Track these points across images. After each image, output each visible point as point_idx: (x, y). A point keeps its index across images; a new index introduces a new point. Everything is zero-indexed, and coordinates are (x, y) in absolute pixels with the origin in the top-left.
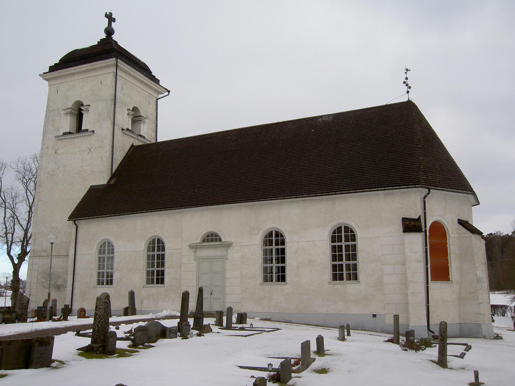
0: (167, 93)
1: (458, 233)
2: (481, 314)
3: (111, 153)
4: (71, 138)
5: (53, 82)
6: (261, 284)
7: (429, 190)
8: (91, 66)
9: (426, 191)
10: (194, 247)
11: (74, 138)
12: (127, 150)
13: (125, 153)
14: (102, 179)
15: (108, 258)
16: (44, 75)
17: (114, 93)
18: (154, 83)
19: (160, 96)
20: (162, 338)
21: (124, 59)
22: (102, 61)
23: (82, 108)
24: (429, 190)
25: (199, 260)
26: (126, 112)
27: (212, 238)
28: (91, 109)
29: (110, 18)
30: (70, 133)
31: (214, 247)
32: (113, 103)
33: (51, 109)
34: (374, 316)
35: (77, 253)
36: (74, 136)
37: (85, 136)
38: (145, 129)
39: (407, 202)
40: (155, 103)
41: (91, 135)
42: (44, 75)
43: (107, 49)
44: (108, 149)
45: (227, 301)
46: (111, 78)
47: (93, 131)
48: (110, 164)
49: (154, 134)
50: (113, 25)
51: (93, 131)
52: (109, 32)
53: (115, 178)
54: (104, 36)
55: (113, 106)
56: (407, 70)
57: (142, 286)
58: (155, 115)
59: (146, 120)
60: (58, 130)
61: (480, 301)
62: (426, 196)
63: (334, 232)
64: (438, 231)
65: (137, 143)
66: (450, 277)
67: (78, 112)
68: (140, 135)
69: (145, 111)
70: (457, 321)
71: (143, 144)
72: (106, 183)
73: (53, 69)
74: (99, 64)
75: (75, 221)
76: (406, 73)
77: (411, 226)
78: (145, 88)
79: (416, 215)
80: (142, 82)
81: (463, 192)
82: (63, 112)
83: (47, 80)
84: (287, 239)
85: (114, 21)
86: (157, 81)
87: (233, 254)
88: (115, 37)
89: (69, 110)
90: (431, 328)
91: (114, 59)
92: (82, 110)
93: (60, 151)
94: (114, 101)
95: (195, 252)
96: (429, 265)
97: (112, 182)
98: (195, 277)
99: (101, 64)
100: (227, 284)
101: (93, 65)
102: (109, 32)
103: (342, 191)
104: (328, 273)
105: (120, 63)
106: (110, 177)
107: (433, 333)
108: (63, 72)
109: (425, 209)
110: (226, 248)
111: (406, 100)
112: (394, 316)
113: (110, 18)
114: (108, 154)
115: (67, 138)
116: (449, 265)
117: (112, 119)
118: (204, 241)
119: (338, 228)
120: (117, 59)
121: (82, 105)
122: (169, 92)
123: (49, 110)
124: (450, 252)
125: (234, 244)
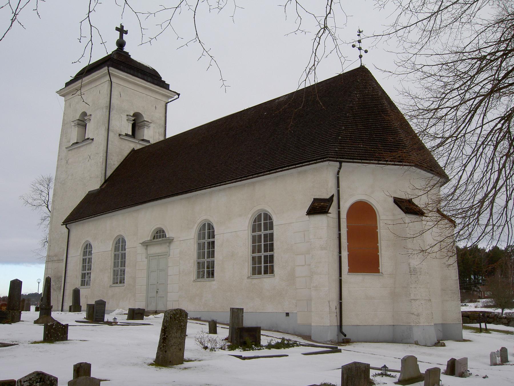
0: (177, 96)
1: (394, 215)
2: (413, 314)
3: (105, 158)
4: (78, 148)
6: (194, 281)
7: (341, 163)
9: (338, 164)
10: (146, 245)
11: (80, 147)
13: (124, 157)
14: (96, 185)
16: (61, 93)
17: (109, 100)
18: (159, 88)
20: (287, 348)
21: (122, 67)
24: (341, 163)
25: (149, 257)
26: (125, 118)
27: (159, 235)
28: (92, 118)
29: (121, 30)
31: (161, 244)
32: (108, 110)
34: (287, 314)
35: (69, 256)
39: (316, 179)
41: (90, 143)
42: (61, 93)
43: (120, 60)
45: (168, 299)
48: (104, 169)
51: (93, 139)
52: (121, 44)
55: (108, 113)
56: (360, 32)
57: (109, 285)
58: (163, 119)
60: (69, 142)
61: (412, 297)
62: (338, 173)
64: (363, 212)
65: (138, 147)
66: (380, 268)
67: (82, 122)
70: (389, 321)
71: (141, 147)
74: (97, 75)
76: (359, 35)
77: (319, 207)
78: (150, 94)
79: (327, 194)
80: (150, 90)
81: (396, 163)
83: (63, 96)
86: (165, 86)
87: (175, 249)
88: (126, 49)
90: (344, 330)
91: (106, 68)
93: (70, 161)
95: (146, 249)
96: (345, 254)
98: (146, 276)
100: (169, 282)
101: (92, 77)
102: (121, 44)
103: (258, 174)
104: (247, 267)
106: (103, 181)
107: (345, 336)
109: (338, 186)
110: (168, 244)
111: (359, 66)
112: (232, 310)
113: (121, 30)
116: (379, 254)
118: (154, 238)
120: (108, 67)
122: (179, 95)
123: (64, 124)
124: (380, 239)
125: (175, 240)
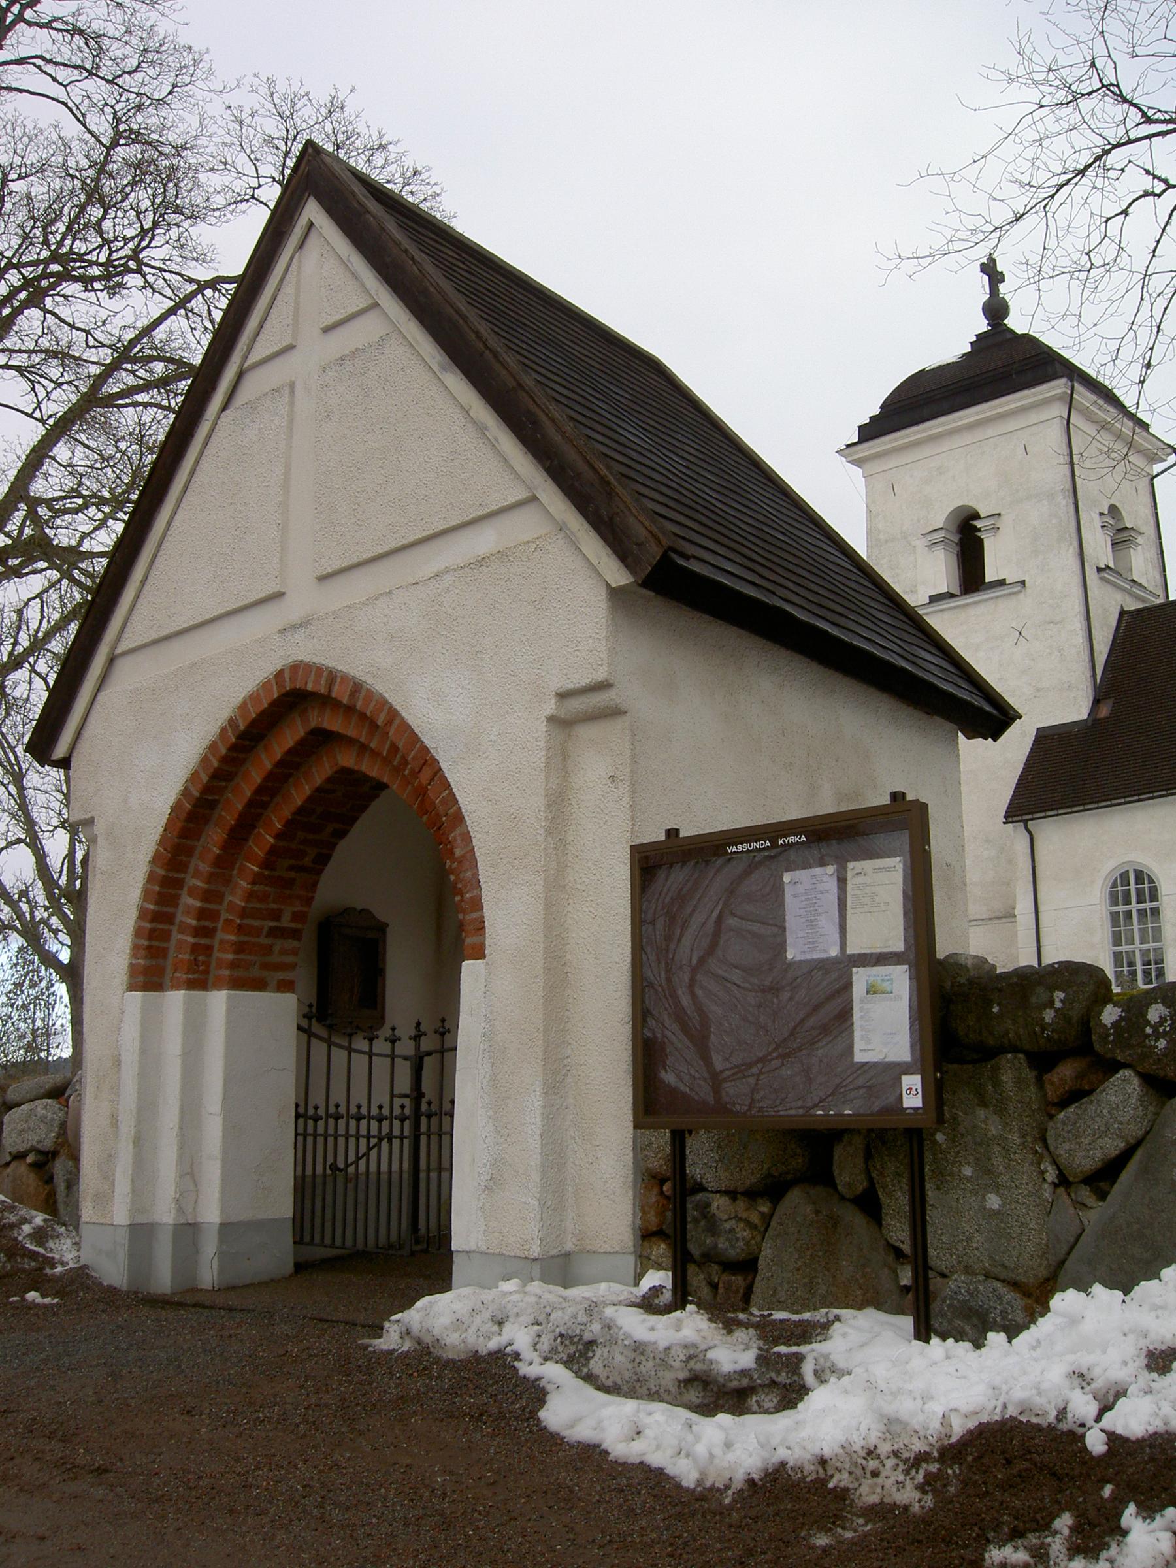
4: (955, 608)
5: (875, 467)
8: (992, 408)
12: (1114, 624)
15: (1142, 913)
19: (1157, 468)
22: (1026, 392)
23: (978, 524)
28: (1005, 523)
29: (991, 271)
30: (951, 595)
32: (1071, 501)
33: (882, 537)
35: (1041, 908)
36: (976, 599)
37: (997, 597)
38: (1140, 563)
40: (1149, 489)
43: (1004, 364)
44: (1077, 624)
46: (1053, 434)
47: (1023, 583)
49: (1158, 577)
50: (1003, 288)
52: (996, 310)
53: (1110, 702)
54: (983, 326)
55: (1072, 507)
59: (1140, 540)
63: (1114, 885)
65: (1132, 605)
68: (1133, 581)
69: (1135, 515)
71: (1140, 606)
72: (1085, 717)
73: (870, 431)
74: (1016, 401)
75: (1026, 822)
82: (920, 543)
83: (858, 463)
84: (1164, 889)
85: (1003, 281)
89: (940, 535)
91: (1064, 380)
92: (979, 530)
94: (1072, 495)
97: (1104, 711)
99: (1021, 399)
102: (996, 310)
105: (1079, 394)
108: (907, 436)
114: (1080, 639)
115: (942, 610)
117: (1076, 543)
119: (1121, 875)
121: (976, 516)
